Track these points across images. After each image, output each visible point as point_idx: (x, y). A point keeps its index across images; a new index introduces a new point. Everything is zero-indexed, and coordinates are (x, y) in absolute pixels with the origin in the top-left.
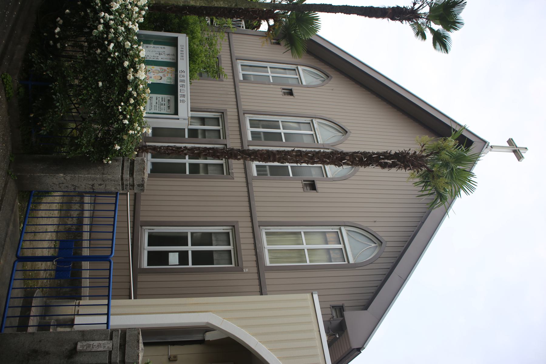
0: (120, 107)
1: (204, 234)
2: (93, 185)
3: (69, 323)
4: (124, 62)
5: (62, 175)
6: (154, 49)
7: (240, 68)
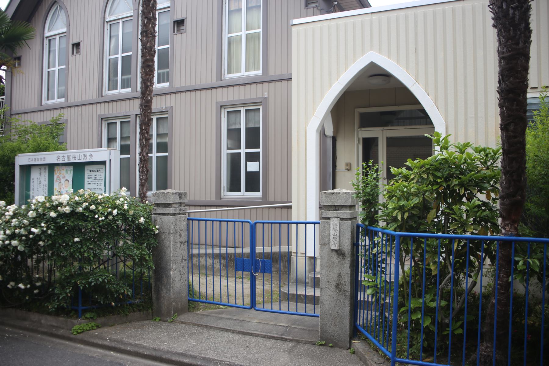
0: (100, 219)
1: (229, 137)
2: (181, 243)
3: (313, 261)
4: (51, 217)
5: (172, 273)
6: (35, 189)
7: (51, 102)
